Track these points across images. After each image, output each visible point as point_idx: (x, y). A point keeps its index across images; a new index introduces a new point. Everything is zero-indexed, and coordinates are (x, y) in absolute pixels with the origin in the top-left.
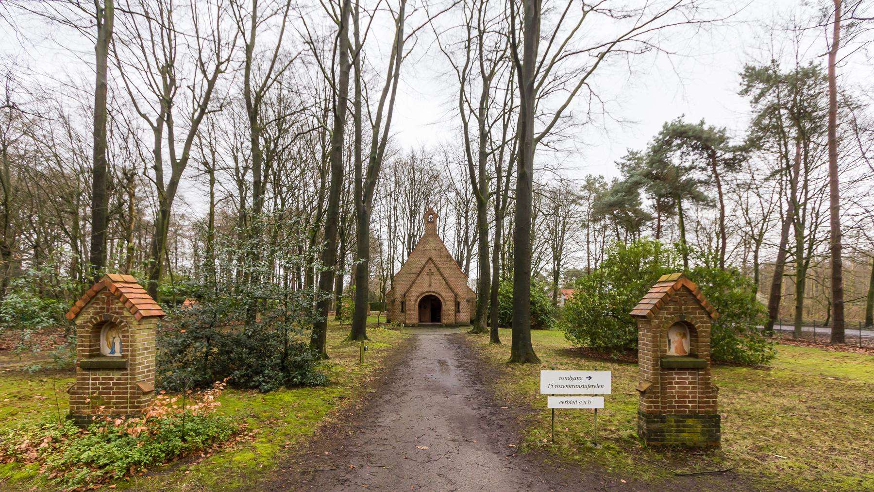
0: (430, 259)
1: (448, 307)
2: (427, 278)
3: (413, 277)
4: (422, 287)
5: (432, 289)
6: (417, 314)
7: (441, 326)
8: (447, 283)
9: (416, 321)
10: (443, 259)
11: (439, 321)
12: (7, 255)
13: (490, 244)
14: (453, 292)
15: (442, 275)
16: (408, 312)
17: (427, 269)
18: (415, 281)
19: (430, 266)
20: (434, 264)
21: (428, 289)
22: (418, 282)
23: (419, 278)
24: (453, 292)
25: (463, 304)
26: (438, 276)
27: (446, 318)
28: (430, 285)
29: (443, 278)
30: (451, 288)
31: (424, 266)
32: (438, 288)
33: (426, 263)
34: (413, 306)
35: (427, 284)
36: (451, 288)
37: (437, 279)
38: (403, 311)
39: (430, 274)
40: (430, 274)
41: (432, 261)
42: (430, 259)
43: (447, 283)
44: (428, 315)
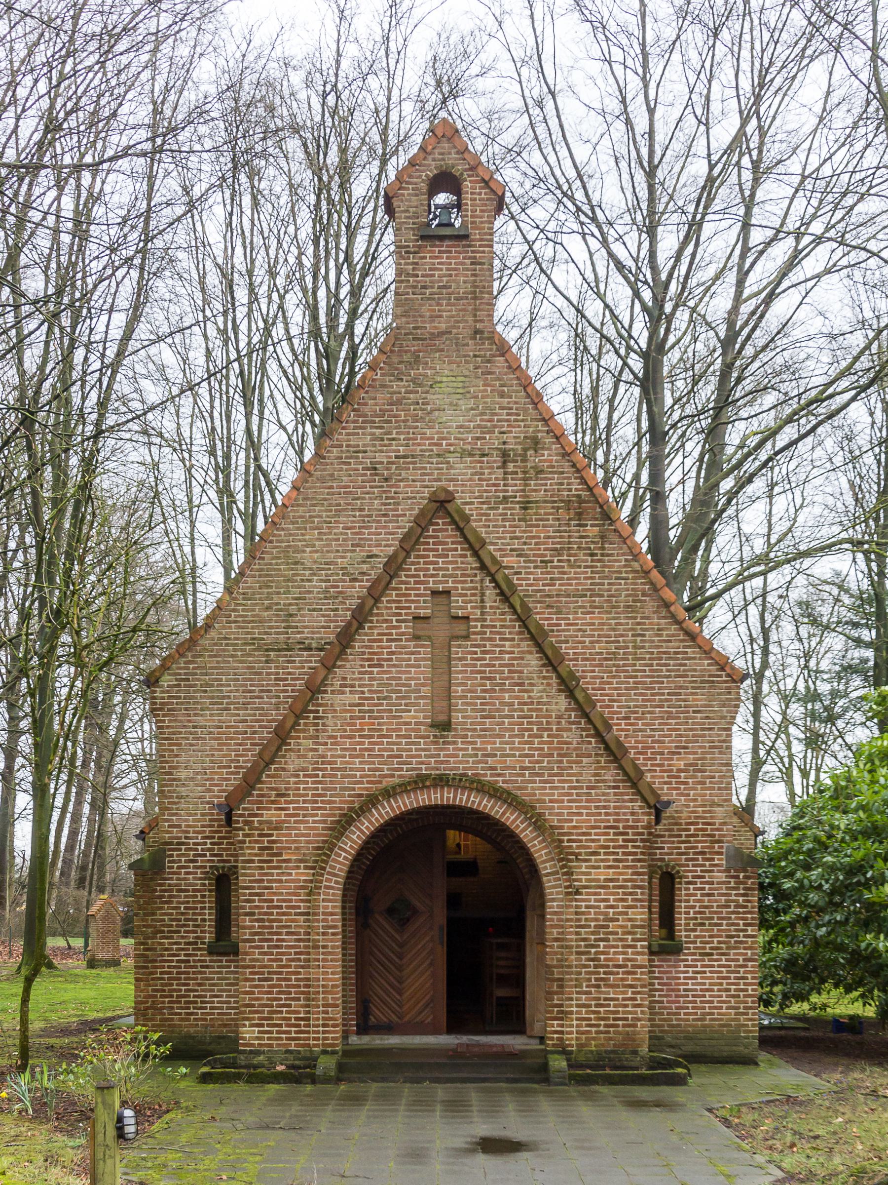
0: (441, 504)
1: (589, 911)
2: (415, 667)
3: (304, 665)
4: (373, 748)
5: (459, 757)
6: (330, 972)
7: (532, 1074)
8: (584, 709)
9: (325, 1025)
10: (547, 531)
11: (513, 1017)
12: (878, 598)
13: (673, 521)
14: (633, 780)
15: (537, 639)
16: (253, 953)
17: (412, 595)
18: (314, 690)
19: (444, 563)
20: (475, 547)
21: (424, 756)
22: (338, 700)
23: (351, 668)
24: (633, 780)
25: (710, 897)
26: (514, 648)
27: (577, 1002)
28: (443, 726)
29: (552, 661)
30: (614, 753)
31: (393, 567)
32: (506, 749)
33: (410, 543)
34: (300, 906)
35: (417, 715)
36: (614, 753)
37: (496, 671)
38: (224, 943)
39: (443, 627)
40: (443, 627)
41: (460, 525)
42: (441, 504)
43: (584, 709)
44: (424, 971)
